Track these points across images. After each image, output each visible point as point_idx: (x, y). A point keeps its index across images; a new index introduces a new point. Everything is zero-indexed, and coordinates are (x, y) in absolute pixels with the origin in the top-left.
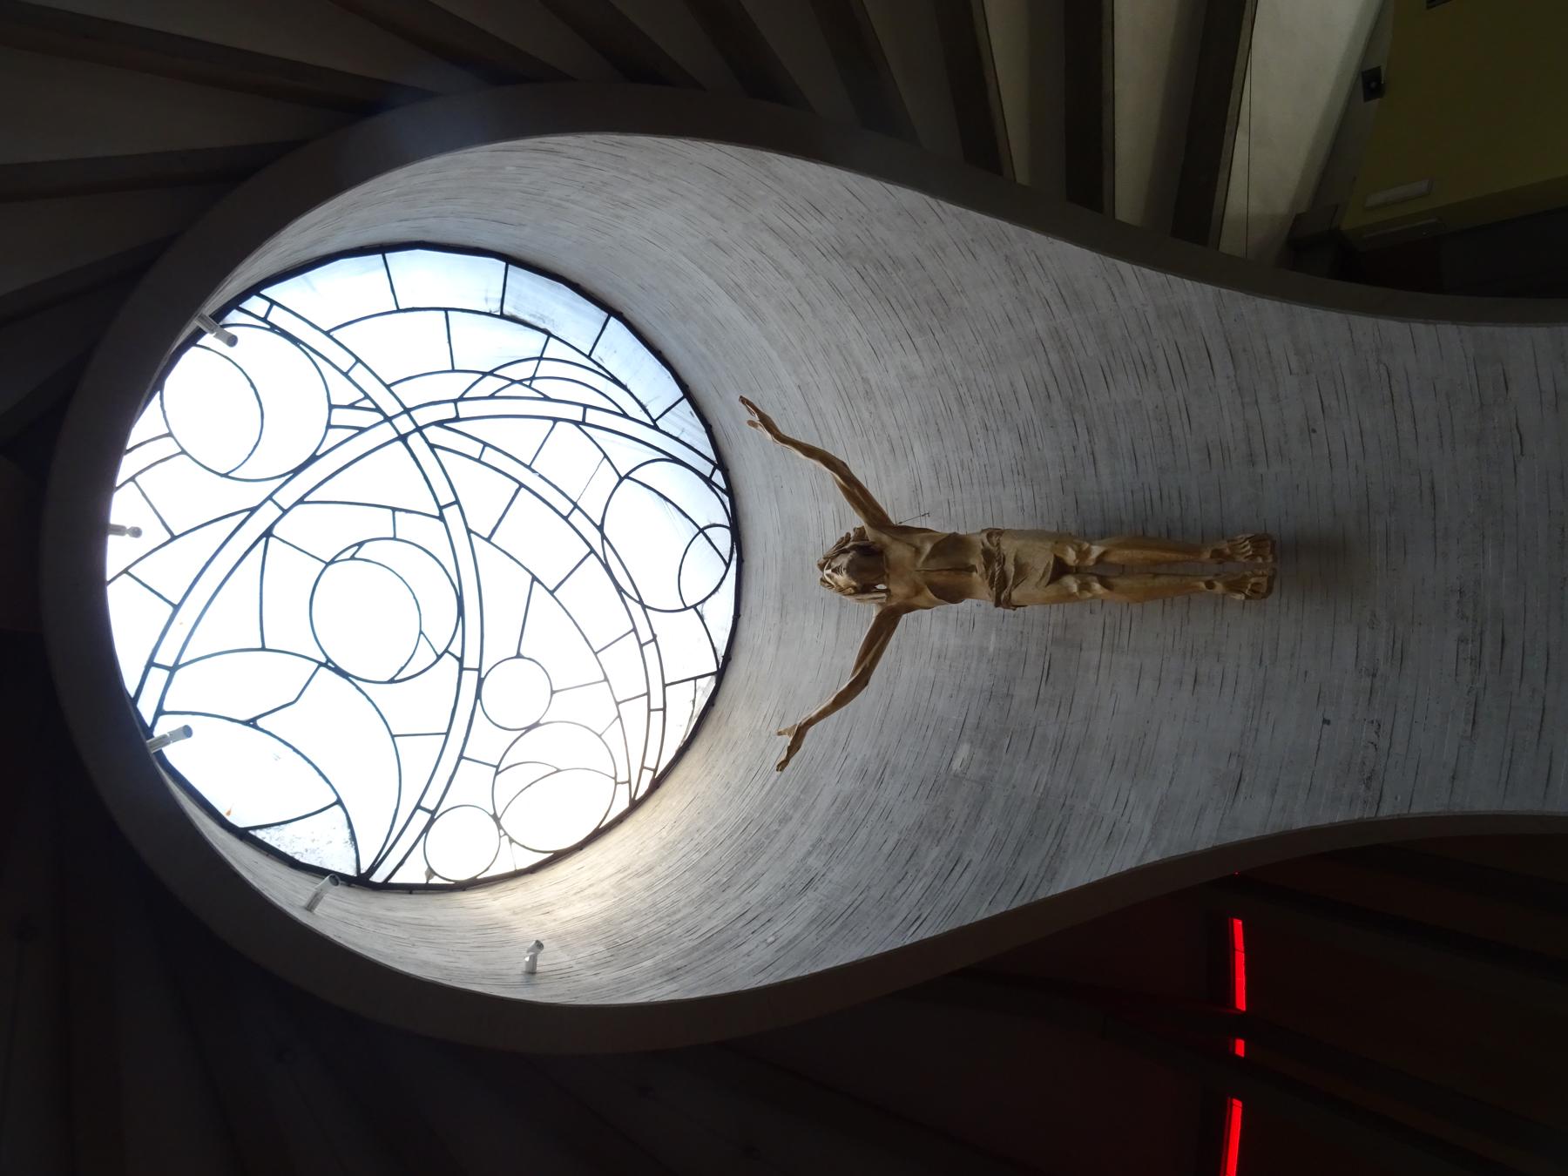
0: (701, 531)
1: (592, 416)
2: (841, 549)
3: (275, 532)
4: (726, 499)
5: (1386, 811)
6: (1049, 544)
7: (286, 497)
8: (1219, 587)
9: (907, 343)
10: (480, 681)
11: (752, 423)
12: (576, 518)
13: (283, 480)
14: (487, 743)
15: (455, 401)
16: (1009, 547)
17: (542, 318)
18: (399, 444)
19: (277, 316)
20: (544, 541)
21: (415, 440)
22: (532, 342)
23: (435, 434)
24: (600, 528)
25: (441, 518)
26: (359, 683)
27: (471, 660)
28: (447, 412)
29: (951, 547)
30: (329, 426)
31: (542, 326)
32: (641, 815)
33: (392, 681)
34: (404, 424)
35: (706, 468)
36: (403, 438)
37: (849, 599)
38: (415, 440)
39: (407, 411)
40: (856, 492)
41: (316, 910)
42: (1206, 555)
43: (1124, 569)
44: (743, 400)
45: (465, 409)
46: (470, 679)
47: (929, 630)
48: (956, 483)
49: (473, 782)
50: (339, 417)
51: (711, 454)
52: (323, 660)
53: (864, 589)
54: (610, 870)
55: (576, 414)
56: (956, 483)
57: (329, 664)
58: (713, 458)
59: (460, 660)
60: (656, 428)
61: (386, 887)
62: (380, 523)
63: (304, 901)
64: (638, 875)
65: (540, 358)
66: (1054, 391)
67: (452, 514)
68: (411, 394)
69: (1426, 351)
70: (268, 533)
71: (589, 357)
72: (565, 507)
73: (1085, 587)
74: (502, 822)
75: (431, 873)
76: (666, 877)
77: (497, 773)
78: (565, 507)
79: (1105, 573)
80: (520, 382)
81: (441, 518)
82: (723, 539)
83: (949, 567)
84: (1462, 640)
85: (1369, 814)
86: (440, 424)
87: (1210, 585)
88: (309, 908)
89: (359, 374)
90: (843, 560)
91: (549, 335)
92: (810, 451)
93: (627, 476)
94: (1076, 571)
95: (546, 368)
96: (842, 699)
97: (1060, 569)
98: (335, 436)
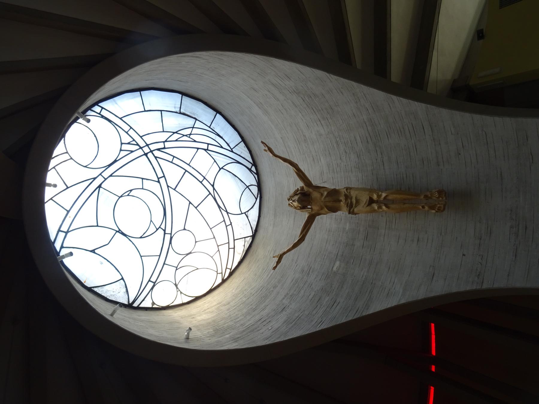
0: (248, 187)
1: (211, 148)
2: (295, 194)
4: (256, 176)
5: (485, 286)
6: (367, 193)
7: (106, 174)
8: (427, 208)
9: (319, 123)
10: (171, 238)
11: (265, 150)
12: (205, 182)
13: (105, 168)
14: (173, 259)
15: (164, 142)
16: (353, 194)
17: (194, 114)
18: (145, 156)
19: (104, 113)
20: (193, 189)
21: (150, 155)
23: (157, 153)
24: (213, 186)
25: (159, 182)
26: (130, 238)
27: (168, 231)
28: (161, 145)
29: (334, 193)
30: (121, 150)
31: (194, 116)
32: (226, 285)
33: (141, 237)
34: (146, 150)
35: (249, 166)
36: (146, 154)
37: (298, 211)
38: (150, 155)
39: (147, 145)
42: (422, 197)
43: (393, 202)
44: (262, 142)
45: (167, 145)
46: (168, 237)
47: (326, 222)
48: (335, 171)
49: (168, 273)
50: (124, 147)
51: (251, 161)
52: (118, 230)
54: (215, 303)
56: (335, 171)
58: (252, 162)
59: (165, 230)
60: (232, 151)
61: (138, 308)
64: (225, 305)
65: (193, 128)
66: (369, 140)
67: (162, 180)
68: (149, 139)
69: (499, 126)
70: (100, 187)
71: (210, 127)
72: (201, 178)
73: (380, 207)
75: (153, 303)
76: (234, 306)
77: (177, 269)
78: (201, 178)
79: (387, 203)
80: (186, 136)
81: (159, 182)
82: (255, 190)
83: (333, 200)
84: (511, 227)
85: (479, 287)
86: (159, 150)
87: (423, 207)
88: (112, 315)
89: (131, 132)
90: (296, 198)
91: (196, 119)
92: (285, 160)
93: (222, 168)
94: (377, 202)
95: (195, 131)
96: (295, 245)
97: (371, 201)
98: (123, 154)
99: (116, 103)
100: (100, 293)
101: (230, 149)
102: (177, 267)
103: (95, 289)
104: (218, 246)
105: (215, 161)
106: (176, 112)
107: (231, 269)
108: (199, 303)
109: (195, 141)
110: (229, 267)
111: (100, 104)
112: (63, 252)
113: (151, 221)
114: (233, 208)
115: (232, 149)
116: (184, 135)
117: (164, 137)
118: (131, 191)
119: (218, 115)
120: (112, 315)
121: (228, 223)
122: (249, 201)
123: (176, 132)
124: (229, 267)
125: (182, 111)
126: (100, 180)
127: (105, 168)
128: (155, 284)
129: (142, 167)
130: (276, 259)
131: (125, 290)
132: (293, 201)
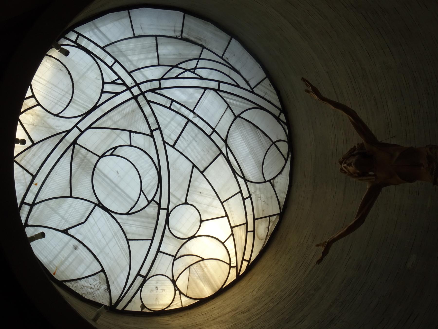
0: (274, 143)
1: (223, 87)
2: (351, 154)
3: (78, 142)
4: (286, 127)
7: (83, 126)
10: (168, 215)
11: (307, 91)
12: (214, 137)
13: (80, 118)
14: (170, 246)
15: (159, 80)
17: (200, 39)
18: (133, 101)
19: (84, 43)
20: (196, 147)
21: (140, 98)
22: (195, 51)
23: (150, 96)
24: (225, 141)
25: (152, 136)
26: (113, 214)
27: (164, 205)
28: (156, 85)
30: (103, 92)
31: (200, 43)
32: (242, 283)
33: (128, 214)
34: (136, 91)
35: (276, 112)
36: (135, 98)
37: (354, 179)
38: (140, 98)
39: (137, 85)
40: (360, 126)
41: (97, 322)
44: (304, 80)
45: (165, 83)
46: (163, 213)
47: (395, 196)
49: (163, 265)
50: (107, 88)
51: (279, 105)
52: (97, 202)
53: (362, 175)
54: (228, 310)
55: (214, 85)
57: (100, 205)
58: (280, 107)
59: (159, 204)
60: (253, 92)
61: (124, 312)
62: (124, 138)
63: (92, 317)
64: (243, 313)
65: (199, 59)
67: (156, 134)
68: (139, 77)
70: (75, 142)
71: (222, 58)
72: (208, 130)
74: (177, 283)
75: (143, 306)
76: (257, 314)
77: (175, 260)
78: (208, 130)
80: (189, 70)
81: (152, 136)
82: (284, 147)
86: (152, 91)
88: (95, 320)
89: (117, 67)
90: (353, 160)
91: (203, 47)
92: (337, 105)
93: (239, 116)
95: (202, 64)
96: (351, 229)
98: (105, 97)
99: (97, 28)
100: (73, 289)
101: (249, 89)
102: (175, 257)
103: (68, 284)
104: (232, 228)
105: (229, 106)
106: (176, 38)
107: (249, 261)
108: (205, 308)
109: (201, 78)
110: (247, 257)
111: (76, 29)
112: (30, 232)
113: (141, 191)
114: (252, 172)
115: (252, 89)
116: (186, 70)
117: (158, 72)
118: (115, 148)
119: (233, 41)
120: (95, 320)
121: (246, 194)
122: (275, 164)
123: (176, 66)
124: (247, 257)
125: (184, 35)
126: (76, 132)
127: (80, 118)
128: (145, 279)
129: (128, 114)
130: (322, 249)
131: (105, 286)
132: (349, 165)
